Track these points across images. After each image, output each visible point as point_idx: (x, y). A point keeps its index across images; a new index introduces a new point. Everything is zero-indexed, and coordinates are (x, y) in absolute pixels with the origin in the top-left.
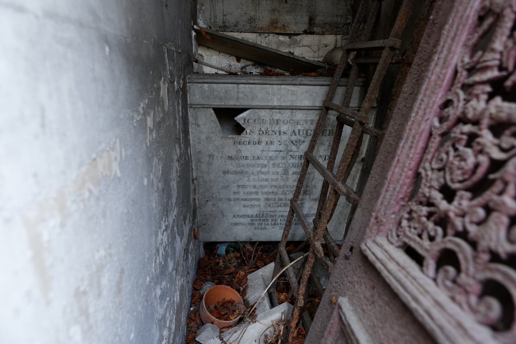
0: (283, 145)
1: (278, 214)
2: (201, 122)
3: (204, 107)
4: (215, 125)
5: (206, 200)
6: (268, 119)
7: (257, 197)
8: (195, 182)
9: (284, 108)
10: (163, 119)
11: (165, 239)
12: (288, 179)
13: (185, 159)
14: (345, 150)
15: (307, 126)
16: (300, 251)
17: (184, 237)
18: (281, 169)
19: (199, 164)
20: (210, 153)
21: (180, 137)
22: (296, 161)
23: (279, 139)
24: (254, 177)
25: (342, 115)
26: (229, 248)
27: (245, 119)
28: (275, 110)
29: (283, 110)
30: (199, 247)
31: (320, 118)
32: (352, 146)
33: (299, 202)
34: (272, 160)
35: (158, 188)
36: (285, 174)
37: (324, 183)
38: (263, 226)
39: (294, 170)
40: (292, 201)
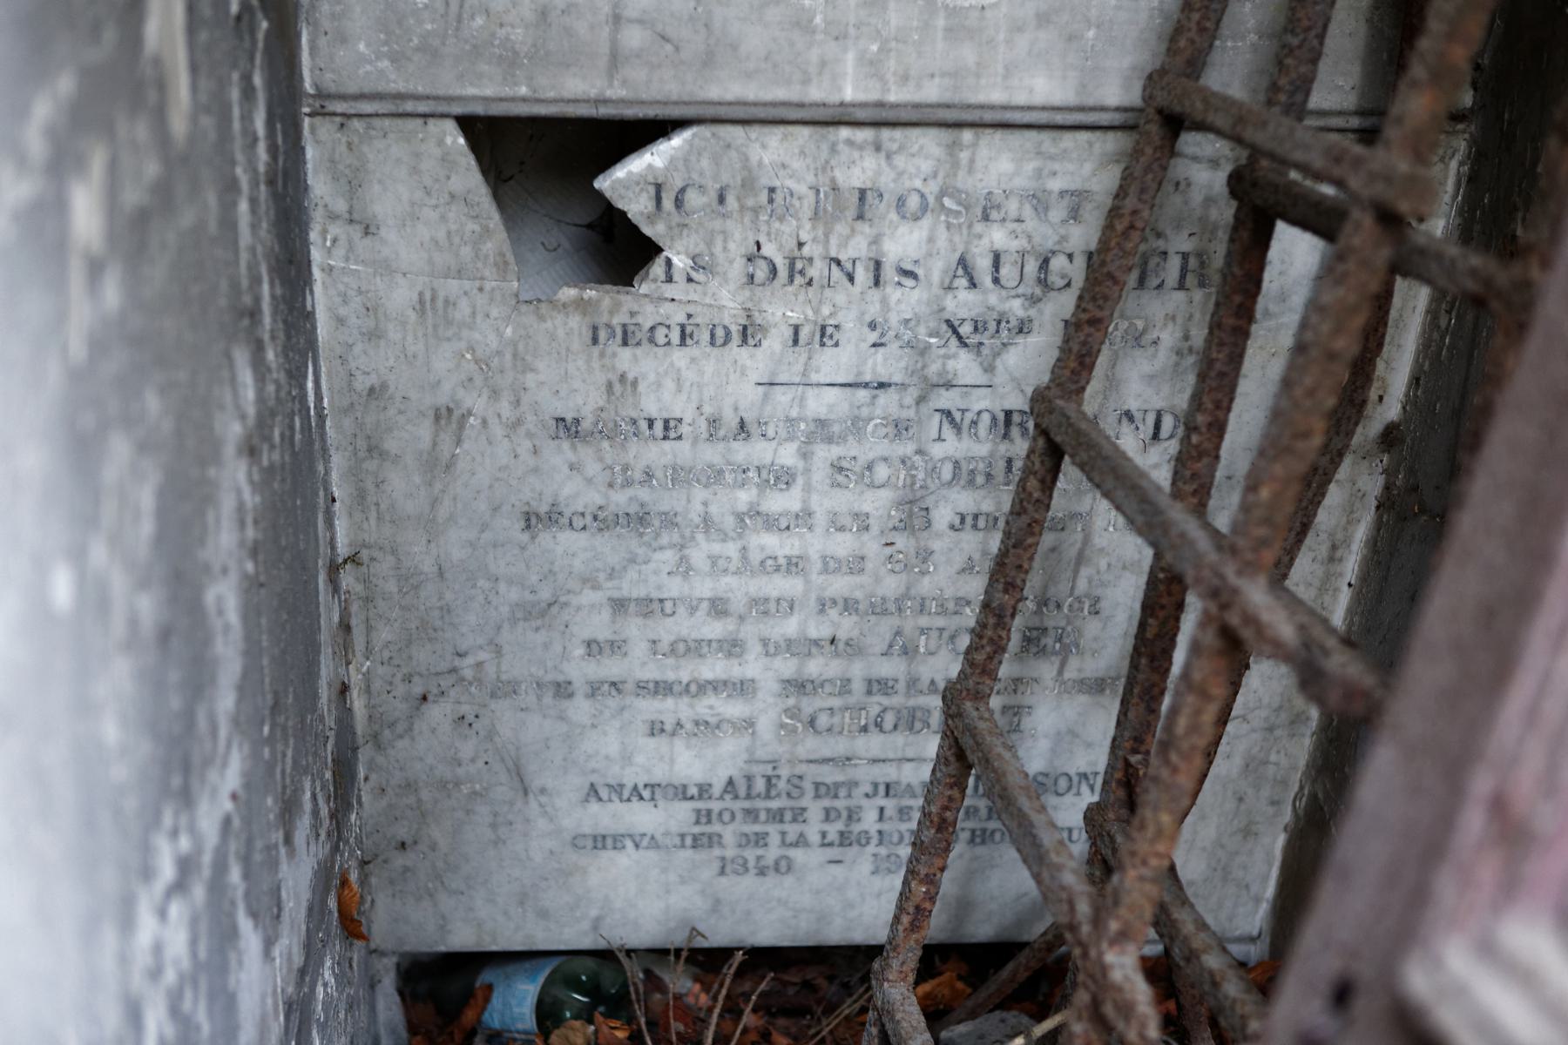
0: (894, 347)
1: (866, 774)
2: (385, 202)
3: (404, 109)
4: (472, 226)
5: (418, 690)
6: (801, 189)
7: (736, 671)
8: (347, 579)
9: (904, 115)
10: (163, 192)
11: (177, 943)
12: (925, 555)
13: (288, 439)
14: (1287, 383)
15: (1045, 233)
16: (1003, 1005)
17: (285, 927)
18: (886, 495)
19: (371, 465)
20: (442, 399)
21: (257, 300)
22: (979, 447)
23: (873, 310)
24: (717, 548)
25: (1264, 163)
26: (560, 992)
27: (659, 188)
28: (845, 132)
29: (898, 133)
30: (372, 985)
31: (1127, 177)
32: (1332, 356)
33: (995, 702)
34: (830, 440)
35: (133, 623)
36: (906, 526)
37: (1152, 582)
38: (773, 852)
39: (965, 500)
40: (956, 697)
